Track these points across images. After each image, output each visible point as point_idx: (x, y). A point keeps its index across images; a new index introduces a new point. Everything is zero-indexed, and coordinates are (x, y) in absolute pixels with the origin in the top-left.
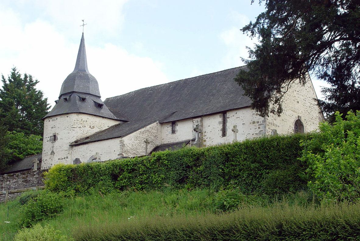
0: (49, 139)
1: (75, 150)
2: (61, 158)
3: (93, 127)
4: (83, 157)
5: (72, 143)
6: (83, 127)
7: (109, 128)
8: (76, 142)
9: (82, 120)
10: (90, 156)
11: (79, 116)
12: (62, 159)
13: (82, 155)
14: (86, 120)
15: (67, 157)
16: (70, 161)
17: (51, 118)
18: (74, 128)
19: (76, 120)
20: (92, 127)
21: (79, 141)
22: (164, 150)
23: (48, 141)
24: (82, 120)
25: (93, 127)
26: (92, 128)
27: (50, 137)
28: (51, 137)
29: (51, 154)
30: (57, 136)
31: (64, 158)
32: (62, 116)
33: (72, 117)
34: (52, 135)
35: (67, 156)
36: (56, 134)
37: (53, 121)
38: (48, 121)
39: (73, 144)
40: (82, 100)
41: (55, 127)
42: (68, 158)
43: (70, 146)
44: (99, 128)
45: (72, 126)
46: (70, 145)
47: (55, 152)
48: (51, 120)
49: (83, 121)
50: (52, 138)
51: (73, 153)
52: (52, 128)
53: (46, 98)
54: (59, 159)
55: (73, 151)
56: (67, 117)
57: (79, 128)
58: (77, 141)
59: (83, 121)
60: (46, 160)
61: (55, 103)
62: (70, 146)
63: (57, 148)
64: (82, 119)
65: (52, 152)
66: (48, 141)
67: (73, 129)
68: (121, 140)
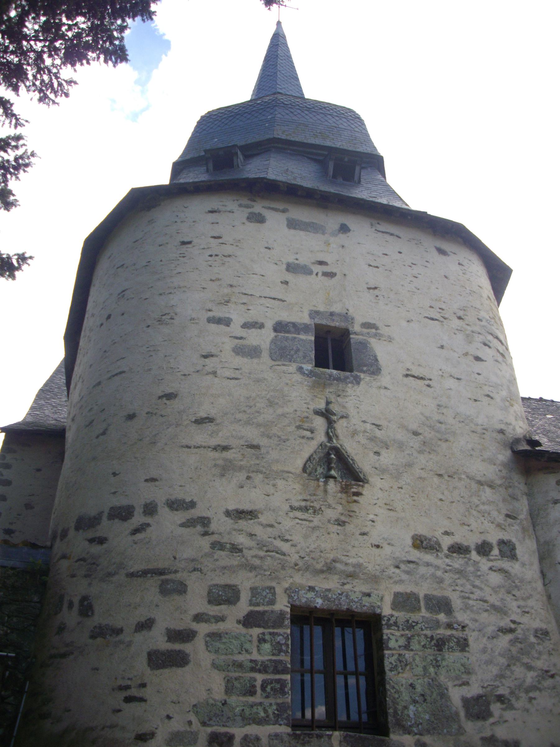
2: (446, 542)
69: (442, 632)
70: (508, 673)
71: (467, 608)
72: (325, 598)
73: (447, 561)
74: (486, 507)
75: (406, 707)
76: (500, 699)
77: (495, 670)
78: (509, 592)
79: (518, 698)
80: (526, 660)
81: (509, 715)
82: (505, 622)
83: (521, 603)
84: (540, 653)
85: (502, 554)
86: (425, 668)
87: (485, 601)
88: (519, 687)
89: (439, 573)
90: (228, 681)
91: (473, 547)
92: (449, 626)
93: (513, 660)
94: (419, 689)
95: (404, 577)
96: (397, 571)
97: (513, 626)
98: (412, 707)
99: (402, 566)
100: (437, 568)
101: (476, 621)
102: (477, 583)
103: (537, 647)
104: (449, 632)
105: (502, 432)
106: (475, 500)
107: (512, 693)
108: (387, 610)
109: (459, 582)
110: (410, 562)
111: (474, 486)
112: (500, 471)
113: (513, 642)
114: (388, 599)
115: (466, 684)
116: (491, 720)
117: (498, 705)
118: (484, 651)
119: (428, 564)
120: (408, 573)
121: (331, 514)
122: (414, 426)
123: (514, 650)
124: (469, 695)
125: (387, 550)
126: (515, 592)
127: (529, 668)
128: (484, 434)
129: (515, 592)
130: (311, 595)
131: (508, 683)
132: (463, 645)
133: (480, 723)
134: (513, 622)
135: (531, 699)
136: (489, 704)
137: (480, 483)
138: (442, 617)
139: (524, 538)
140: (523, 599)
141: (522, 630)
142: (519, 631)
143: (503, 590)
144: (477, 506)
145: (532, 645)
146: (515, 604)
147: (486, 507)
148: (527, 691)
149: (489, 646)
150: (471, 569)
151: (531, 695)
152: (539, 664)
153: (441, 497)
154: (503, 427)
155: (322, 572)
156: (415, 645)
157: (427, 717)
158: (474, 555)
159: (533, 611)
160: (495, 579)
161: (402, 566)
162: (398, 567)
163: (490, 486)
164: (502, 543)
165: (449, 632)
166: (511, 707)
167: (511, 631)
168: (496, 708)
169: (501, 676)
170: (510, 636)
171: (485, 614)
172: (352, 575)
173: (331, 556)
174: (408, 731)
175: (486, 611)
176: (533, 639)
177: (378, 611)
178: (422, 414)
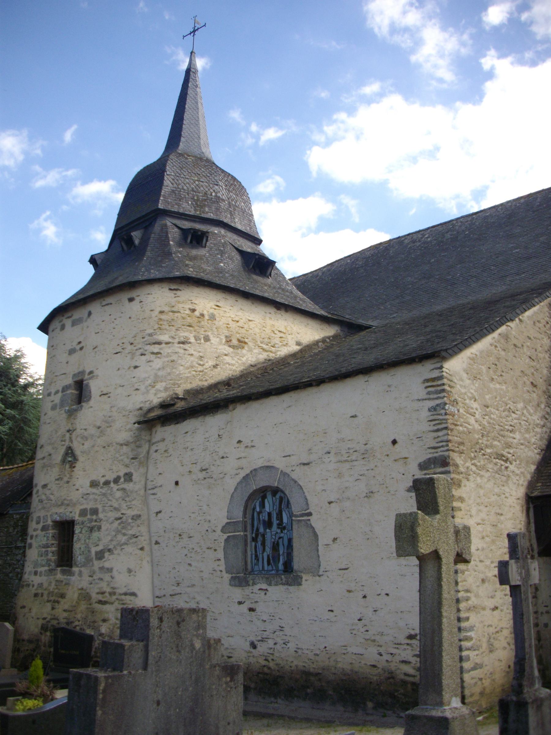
0: (57, 399)
1: (163, 440)
2: (102, 480)
3: (239, 341)
4: (202, 475)
5: (150, 410)
6: (197, 338)
7: (301, 351)
8: (163, 406)
9: (193, 310)
10: (243, 474)
11: (178, 293)
12: (107, 483)
13: (196, 469)
14: (212, 311)
15: (129, 477)
16: (142, 492)
17: (70, 314)
18: (159, 343)
19: (166, 309)
20: (235, 342)
21: (182, 399)
22: (300, 514)
23: (54, 408)
24: (193, 310)
25: (239, 341)
26: (233, 347)
27: (62, 392)
28: (65, 389)
29: (64, 461)
30: (87, 385)
31: (116, 480)
32: (110, 299)
33: (150, 298)
34: (69, 381)
35: (127, 470)
36: (86, 377)
37: (74, 324)
38: (59, 328)
39: (152, 415)
40: (191, 242)
41: (81, 349)
42: (131, 480)
43: (139, 423)
44: (265, 346)
45: (150, 335)
46: (142, 419)
47: (78, 452)
48: (68, 323)
49: (197, 313)
50: (69, 392)
51: (153, 455)
52: (72, 352)
53: (75, 327)
54: (94, 484)
55: (154, 448)
56: (131, 300)
57: (179, 343)
58: (172, 399)
59: (197, 313)
60: (45, 486)
61: (90, 271)
62: (139, 423)
63: (86, 434)
64: (192, 307)
65: (66, 454)
66: (54, 408)
67: (156, 348)
68: (435, 374)
69: (94, 524)
70: (115, 538)
71: (104, 511)
72: (60, 516)
73: (101, 490)
74: (122, 458)
75: (78, 557)
76: (109, 550)
77: (109, 538)
78: (123, 500)
79: (116, 549)
80: (124, 531)
81: (111, 557)
82: (119, 515)
83: (129, 504)
84: (132, 527)
85: (125, 480)
86: (85, 540)
87: (112, 506)
88: (118, 544)
89: (96, 497)
90: (39, 552)
91: (112, 480)
92: (96, 521)
93: (118, 532)
94: (82, 549)
95: (84, 501)
96: (82, 499)
97: (121, 516)
98: (79, 557)
99: (85, 497)
100: (96, 494)
101: (106, 516)
102: (110, 498)
103: (132, 524)
104: (95, 524)
105: (141, 409)
106: (117, 455)
107: (114, 547)
108: (77, 518)
109: (103, 499)
110: (88, 494)
111: (118, 447)
112: (134, 433)
113: (119, 524)
114: (78, 513)
115: (98, 545)
116: (104, 560)
117: (108, 553)
118: (107, 530)
119: (93, 494)
120: (86, 499)
121: (66, 479)
122: (98, 424)
123: (120, 527)
124: (98, 550)
125: (81, 490)
126: (127, 499)
127: (124, 534)
128: (348, 457)
129: (500, 473)
130: (56, 516)
131: (114, 543)
132: (99, 528)
133: (99, 561)
134: (122, 514)
135: (122, 549)
136: (104, 553)
137: (122, 445)
138: (94, 517)
139: (139, 468)
140: (130, 501)
141: (126, 517)
142: (124, 518)
143: (121, 499)
144: (117, 458)
145: (129, 524)
146: (125, 505)
147: (122, 458)
148: (121, 546)
149: (110, 527)
150: (109, 492)
151: (123, 547)
152: (131, 532)
153: (103, 458)
154: (142, 405)
155: (60, 505)
156: (84, 532)
157: (83, 560)
158: (112, 485)
159: (134, 507)
160: (119, 494)
161: (85, 497)
162: (83, 498)
163: (126, 445)
164: (126, 474)
165: (95, 524)
166: (113, 554)
167: (120, 518)
168: (107, 554)
169: (112, 540)
170: (119, 521)
171: (111, 513)
172: (68, 505)
173: (63, 498)
174: (78, 567)
175: (111, 511)
176: (130, 521)
177: (74, 519)
178: (104, 415)
